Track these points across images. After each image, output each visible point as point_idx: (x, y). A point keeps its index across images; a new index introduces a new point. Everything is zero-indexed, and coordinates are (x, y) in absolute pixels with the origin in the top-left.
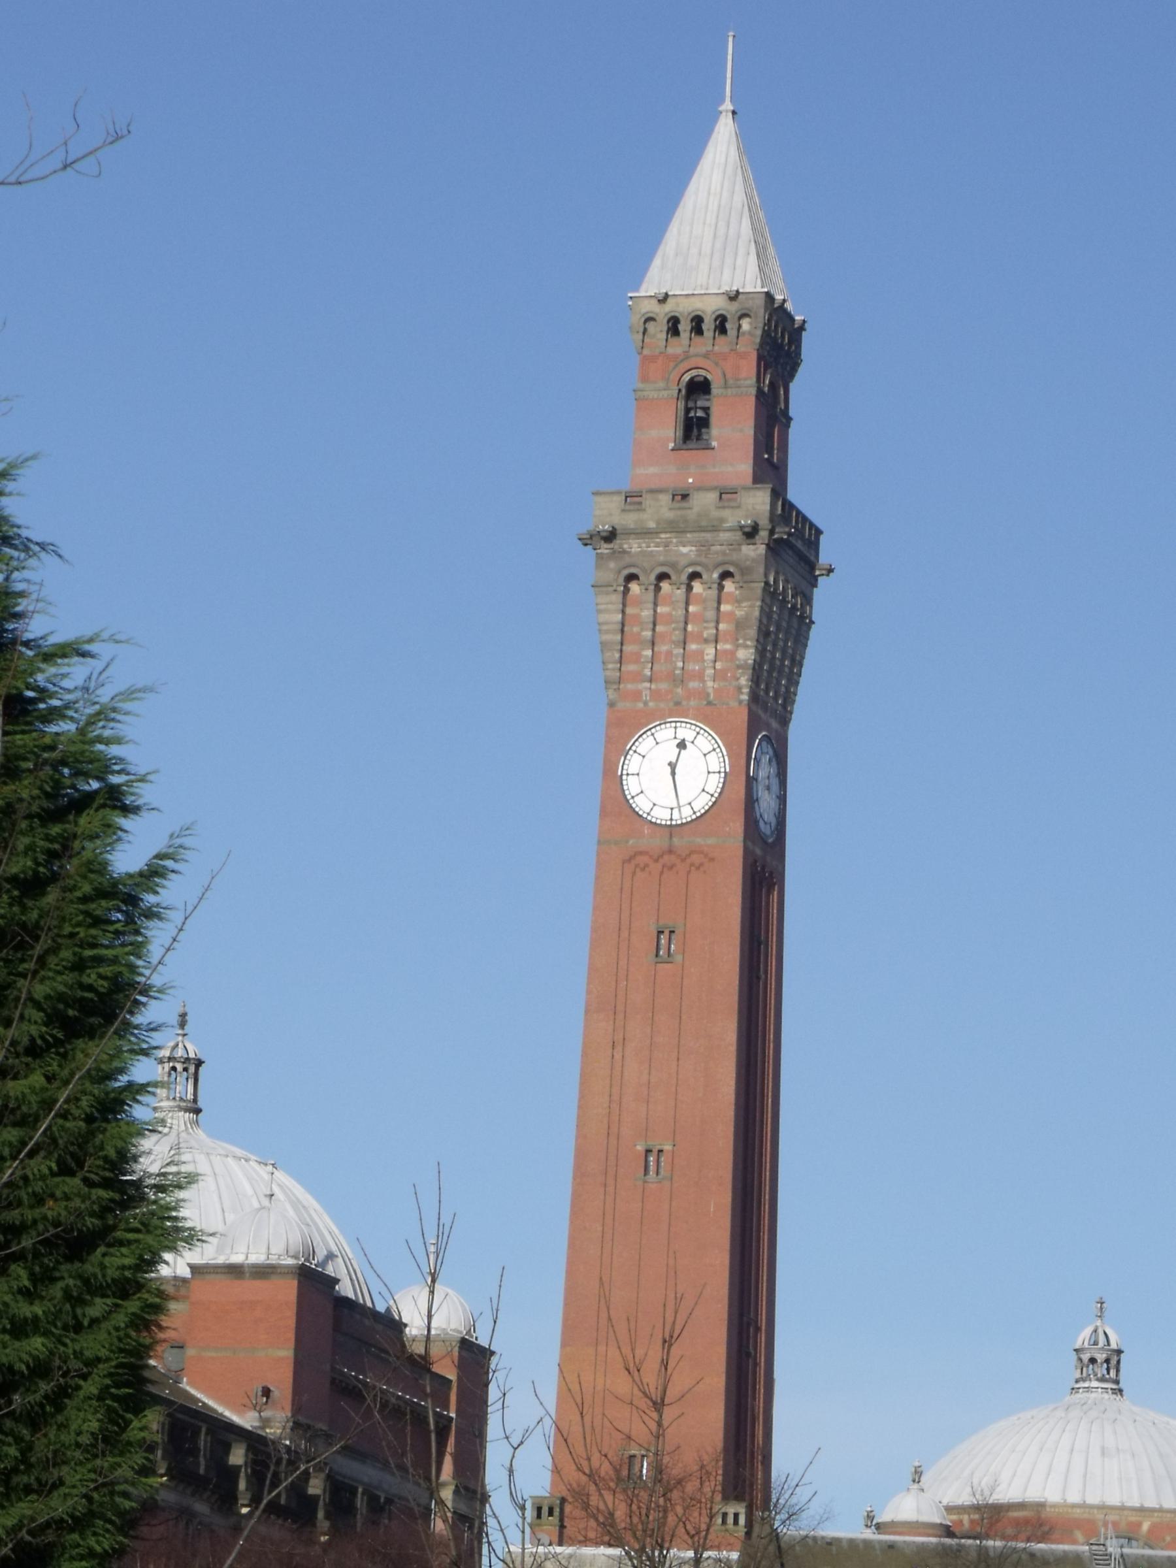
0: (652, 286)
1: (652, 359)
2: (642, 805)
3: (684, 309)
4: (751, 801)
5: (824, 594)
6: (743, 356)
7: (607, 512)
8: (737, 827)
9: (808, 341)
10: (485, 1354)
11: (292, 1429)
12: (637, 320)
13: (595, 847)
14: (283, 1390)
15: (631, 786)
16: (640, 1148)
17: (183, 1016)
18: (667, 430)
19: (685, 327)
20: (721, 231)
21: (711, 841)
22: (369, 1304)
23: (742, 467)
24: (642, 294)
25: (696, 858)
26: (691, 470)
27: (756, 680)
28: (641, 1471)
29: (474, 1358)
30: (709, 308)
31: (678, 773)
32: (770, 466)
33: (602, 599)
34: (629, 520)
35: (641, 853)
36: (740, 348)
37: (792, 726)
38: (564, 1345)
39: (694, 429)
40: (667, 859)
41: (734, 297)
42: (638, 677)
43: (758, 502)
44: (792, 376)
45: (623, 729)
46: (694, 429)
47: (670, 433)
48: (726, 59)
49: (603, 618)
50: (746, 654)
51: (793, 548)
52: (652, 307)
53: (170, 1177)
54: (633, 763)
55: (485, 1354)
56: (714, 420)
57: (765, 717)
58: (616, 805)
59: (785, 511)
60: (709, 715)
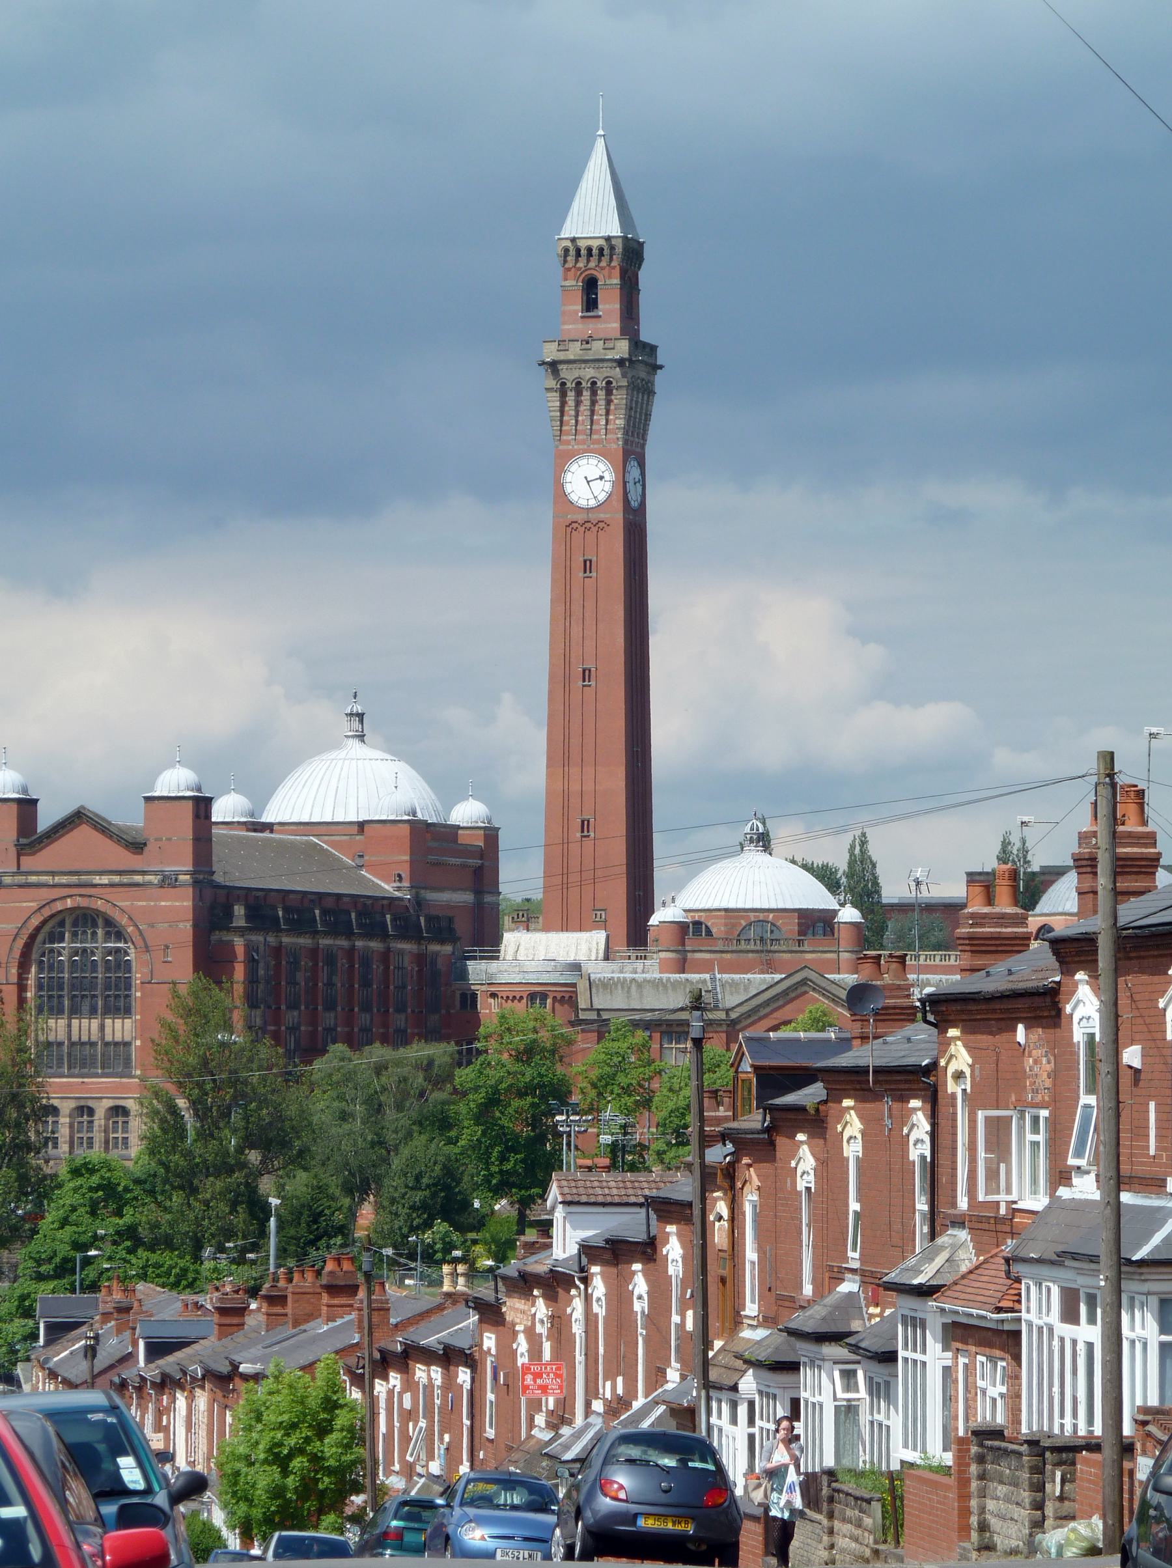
0: (568, 231)
1: (569, 269)
2: (573, 497)
4: (625, 494)
6: (614, 268)
7: (550, 352)
8: (618, 506)
14: (405, 875)
15: (568, 488)
16: (582, 559)
18: (577, 307)
20: (600, 202)
23: (615, 326)
25: (601, 525)
26: (590, 328)
27: (626, 433)
29: (491, 835)
30: (595, 244)
31: (589, 481)
33: (549, 395)
34: (561, 356)
35: (575, 525)
36: (613, 264)
37: (647, 447)
38: (548, 767)
39: (591, 304)
40: (575, 525)
42: (568, 434)
43: (622, 348)
44: (639, 268)
45: (563, 460)
46: (591, 304)
47: (580, 307)
48: (605, 1339)
49: (550, 404)
50: (621, 422)
52: (568, 244)
54: (569, 477)
57: (632, 453)
58: (561, 496)
59: (637, 345)
60: (605, 454)
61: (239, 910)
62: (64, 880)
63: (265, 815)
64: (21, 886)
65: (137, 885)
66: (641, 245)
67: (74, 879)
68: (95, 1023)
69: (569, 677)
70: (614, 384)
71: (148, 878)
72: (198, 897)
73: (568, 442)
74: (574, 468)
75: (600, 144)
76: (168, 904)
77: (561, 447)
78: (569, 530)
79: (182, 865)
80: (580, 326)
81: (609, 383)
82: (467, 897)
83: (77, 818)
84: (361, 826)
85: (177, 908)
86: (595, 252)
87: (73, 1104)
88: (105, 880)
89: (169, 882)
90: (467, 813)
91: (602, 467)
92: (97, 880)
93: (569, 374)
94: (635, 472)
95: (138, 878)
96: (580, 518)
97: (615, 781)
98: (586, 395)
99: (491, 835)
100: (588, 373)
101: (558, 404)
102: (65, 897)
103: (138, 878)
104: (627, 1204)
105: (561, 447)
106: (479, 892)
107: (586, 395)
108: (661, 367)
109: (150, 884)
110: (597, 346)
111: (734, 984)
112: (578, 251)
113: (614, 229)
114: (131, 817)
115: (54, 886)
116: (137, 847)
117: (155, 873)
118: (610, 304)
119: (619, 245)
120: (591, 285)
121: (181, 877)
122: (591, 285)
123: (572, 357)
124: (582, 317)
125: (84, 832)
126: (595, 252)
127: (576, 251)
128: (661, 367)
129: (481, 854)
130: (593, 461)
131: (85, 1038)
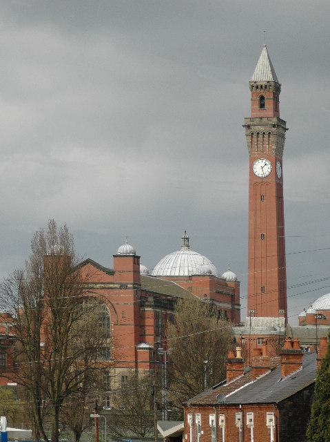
0: (253, 79)
2: (257, 174)
3: (259, 84)
9: (282, 87)
10: (239, 282)
13: (250, 93)
15: (255, 171)
17: (274, 368)
18: (257, 107)
19: (259, 87)
26: (262, 113)
28: (147, 348)
29: (237, 283)
30: (264, 84)
32: (276, 109)
35: (256, 182)
39: (262, 106)
41: (268, 82)
45: (252, 161)
46: (262, 106)
50: (274, 147)
51: (281, 124)
54: (255, 166)
55: (239, 282)
56: (266, 104)
57: (277, 160)
59: (279, 120)
60: (268, 159)
61: (151, 299)
63: (157, 268)
65: (111, 288)
69: (257, 237)
72: (136, 293)
75: (264, 53)
79: (129, 279)
81: (270, 133)
82: (229, 306)
83: (88, 261)
84: (190, 277)
85: (126, 299)
89: (123, 287)
90: (229, 275)
94: (279, 165)
95: (111, 286)
97: (275, 270)
99: (237, 283)
100: (262, 129)
103: (111, 286)
104: (127, 256)
106: (233, 305)
108: (288, 129)
110: (265, 120)
111: (182, 285)
113: (270, 78)
114: (109, 264)
116: (111, 273)
118: (269, 105)
119: (272, 84)
120: (262, 98)
121: (129, 286)
122: (262, 98)
125: (89, 265)
127: (255, 87)
128: (288, 129)
129: (234, 291)
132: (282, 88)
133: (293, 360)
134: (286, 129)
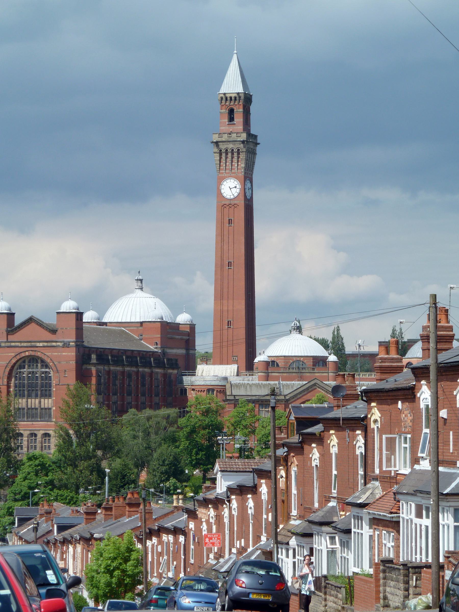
0: (222, 91)
1: (223, 105)
2: (225, 195)
4: (245, 193)
5: (258, 148)
6: (241, 105)
7: (216, 138)
8: (242, 198)
11: (223, 428)
12: (219, 98)
14: (159, 342)
15: (223, 191)
16: (228, 219)
18: (226, 120)
20: (235, 79)
21: (238, 202)
22: (280, 565)
23: (241, 127)
24: (220, 92)
26: (231, 128)
27: (245, 169)
29: (192, 327)
30: (233, 96)
31: (231, 188)
33: (215, 154)
34: (220, 139)
35: (225, 206)
36: (240, 103)
39: (231, 119)
43: (244, 136)
44: (250, 105)
46: (231, 119)
47: (227, 120)
50: (243, 165)
52: (223, 95)
53: (348, 596)
54: (223, 187)
57: (248, 177)
59: (249, 135)
60: (237, 178)
61: (94, 356)
62: (25, 344)
64: (8, 347)
65: (54, 346)
66: (251, 96)
67: (29, 344)
68: (37, 401)
69: (223, 265)
70: (241, 150)
71: (58, 344)
72: (78, 351)
73: (222, 173)
74: (225, 183)
76: (66, 354)
77: (220, 175)
78: (223, 207)
79: (71, 339)
80: (227, 128)
81: (238, 150)
82: (183, 351)
83: (30, 320)
84: (142, 323)
85: (69, 356)
86: (233, 99)
87: (28, 432)
88: (41, 344)
89: (66, 345)
90: (183, 318)
91: (236, 183)
92: (38, 344)
93: (223, 146)
94: (249, 185)
95: (54, 344)
96: (227, 203)
97: (241, 306)
98: (230, 155)
99: (192, 327)
100: (230, 146)
101: (218, 158)
102: (25, 351)
103: (54, 344)
105: (220, 175)
106: (187, 349)
107: (230, 155)
108: (259, 144)
109: (59, 346)
110: (234, 135)
112: (226, 98)
113: (240, 90)
114: (51, 320)
115: (21, 347)
116: (54, 332)
117: (61, 342)
118: (239, 119)
119: (242, 96)
120: (231, 112)
122: (231, 112)
123: (224, 140)
124: (228, 124)
125: (33, 326)
126: (233, 99)
127: (225, 98)
128: (259, 144)
129: (188, 334)
130: (232, 181)
131: (33, 407)
132: (254, 99)
133: (447, 373)
134: (257, 144)
